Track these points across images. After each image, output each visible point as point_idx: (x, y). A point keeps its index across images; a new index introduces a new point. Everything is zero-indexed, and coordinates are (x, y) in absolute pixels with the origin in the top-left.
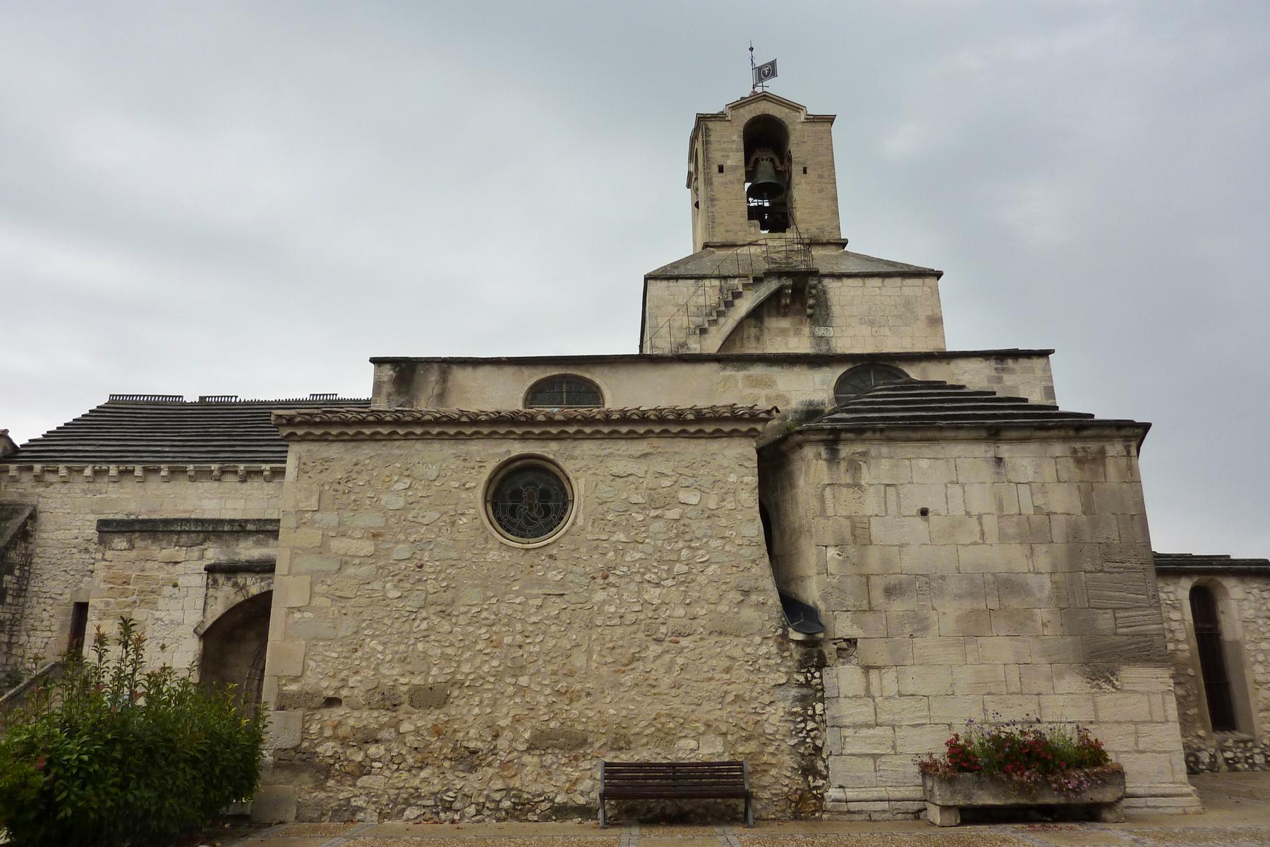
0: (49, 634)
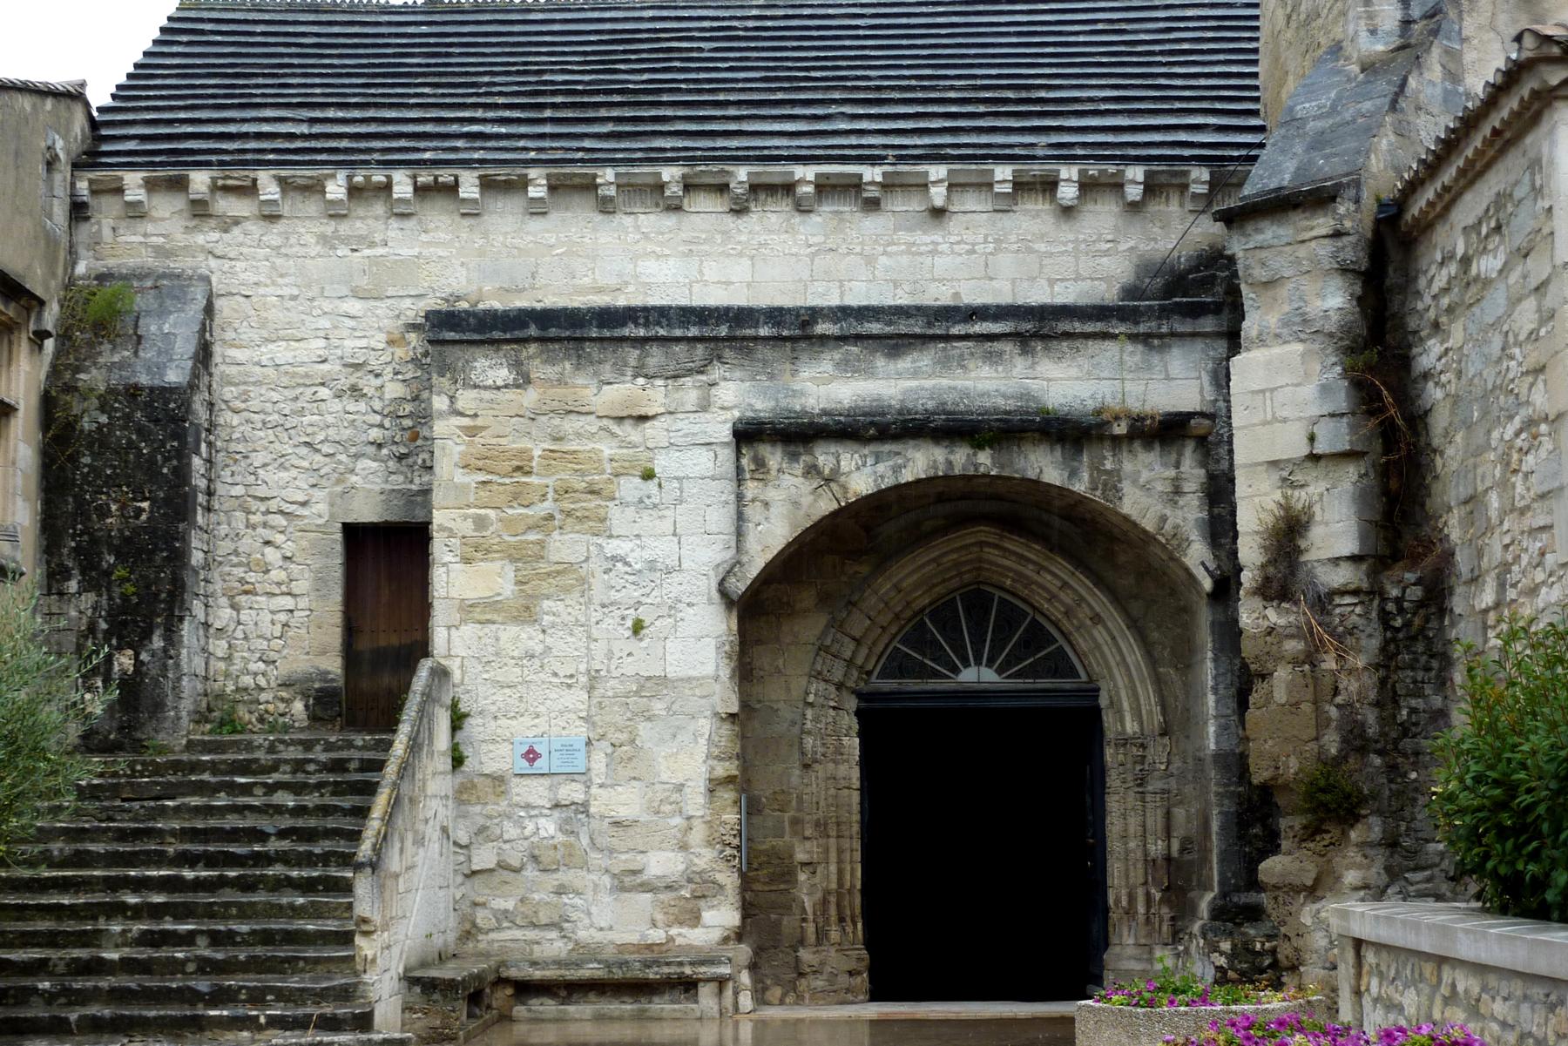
0: (288, 602)
